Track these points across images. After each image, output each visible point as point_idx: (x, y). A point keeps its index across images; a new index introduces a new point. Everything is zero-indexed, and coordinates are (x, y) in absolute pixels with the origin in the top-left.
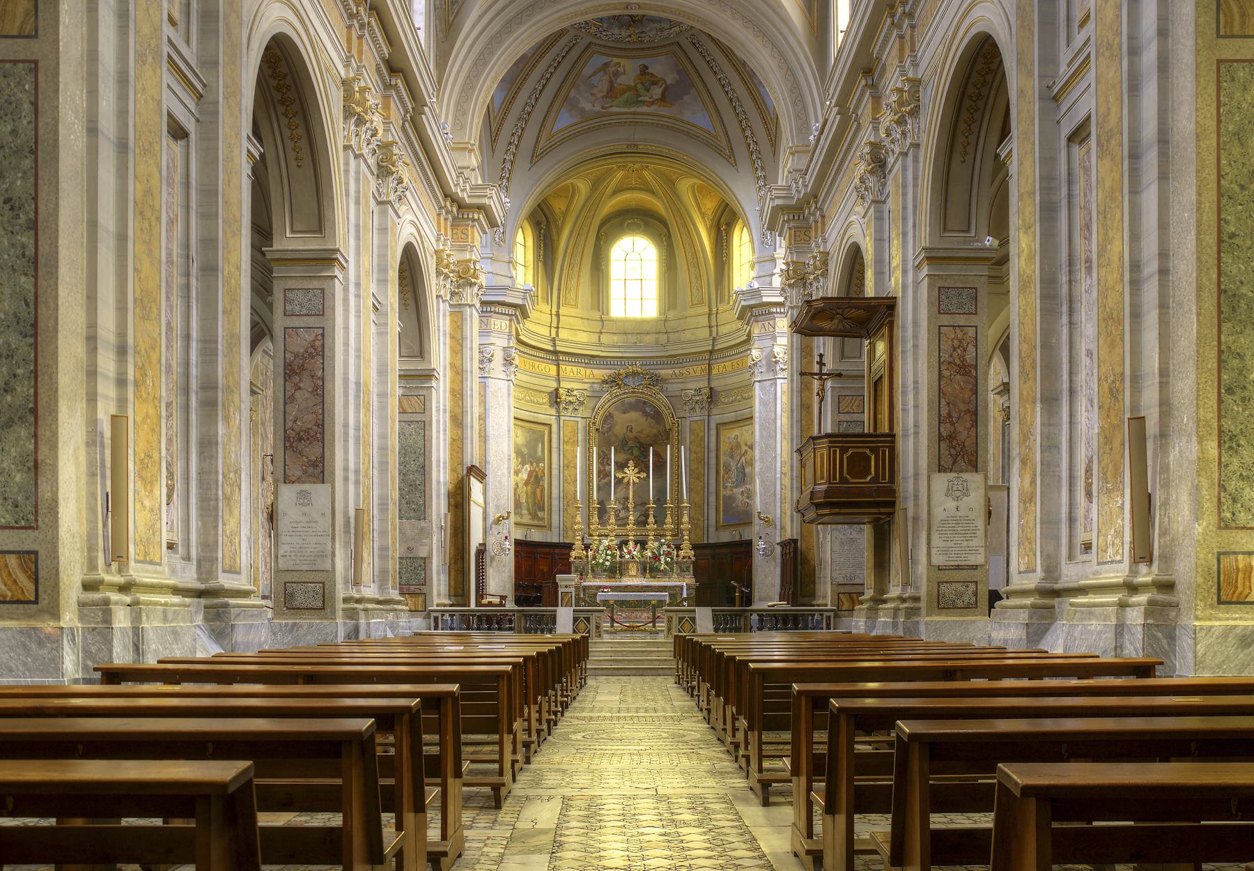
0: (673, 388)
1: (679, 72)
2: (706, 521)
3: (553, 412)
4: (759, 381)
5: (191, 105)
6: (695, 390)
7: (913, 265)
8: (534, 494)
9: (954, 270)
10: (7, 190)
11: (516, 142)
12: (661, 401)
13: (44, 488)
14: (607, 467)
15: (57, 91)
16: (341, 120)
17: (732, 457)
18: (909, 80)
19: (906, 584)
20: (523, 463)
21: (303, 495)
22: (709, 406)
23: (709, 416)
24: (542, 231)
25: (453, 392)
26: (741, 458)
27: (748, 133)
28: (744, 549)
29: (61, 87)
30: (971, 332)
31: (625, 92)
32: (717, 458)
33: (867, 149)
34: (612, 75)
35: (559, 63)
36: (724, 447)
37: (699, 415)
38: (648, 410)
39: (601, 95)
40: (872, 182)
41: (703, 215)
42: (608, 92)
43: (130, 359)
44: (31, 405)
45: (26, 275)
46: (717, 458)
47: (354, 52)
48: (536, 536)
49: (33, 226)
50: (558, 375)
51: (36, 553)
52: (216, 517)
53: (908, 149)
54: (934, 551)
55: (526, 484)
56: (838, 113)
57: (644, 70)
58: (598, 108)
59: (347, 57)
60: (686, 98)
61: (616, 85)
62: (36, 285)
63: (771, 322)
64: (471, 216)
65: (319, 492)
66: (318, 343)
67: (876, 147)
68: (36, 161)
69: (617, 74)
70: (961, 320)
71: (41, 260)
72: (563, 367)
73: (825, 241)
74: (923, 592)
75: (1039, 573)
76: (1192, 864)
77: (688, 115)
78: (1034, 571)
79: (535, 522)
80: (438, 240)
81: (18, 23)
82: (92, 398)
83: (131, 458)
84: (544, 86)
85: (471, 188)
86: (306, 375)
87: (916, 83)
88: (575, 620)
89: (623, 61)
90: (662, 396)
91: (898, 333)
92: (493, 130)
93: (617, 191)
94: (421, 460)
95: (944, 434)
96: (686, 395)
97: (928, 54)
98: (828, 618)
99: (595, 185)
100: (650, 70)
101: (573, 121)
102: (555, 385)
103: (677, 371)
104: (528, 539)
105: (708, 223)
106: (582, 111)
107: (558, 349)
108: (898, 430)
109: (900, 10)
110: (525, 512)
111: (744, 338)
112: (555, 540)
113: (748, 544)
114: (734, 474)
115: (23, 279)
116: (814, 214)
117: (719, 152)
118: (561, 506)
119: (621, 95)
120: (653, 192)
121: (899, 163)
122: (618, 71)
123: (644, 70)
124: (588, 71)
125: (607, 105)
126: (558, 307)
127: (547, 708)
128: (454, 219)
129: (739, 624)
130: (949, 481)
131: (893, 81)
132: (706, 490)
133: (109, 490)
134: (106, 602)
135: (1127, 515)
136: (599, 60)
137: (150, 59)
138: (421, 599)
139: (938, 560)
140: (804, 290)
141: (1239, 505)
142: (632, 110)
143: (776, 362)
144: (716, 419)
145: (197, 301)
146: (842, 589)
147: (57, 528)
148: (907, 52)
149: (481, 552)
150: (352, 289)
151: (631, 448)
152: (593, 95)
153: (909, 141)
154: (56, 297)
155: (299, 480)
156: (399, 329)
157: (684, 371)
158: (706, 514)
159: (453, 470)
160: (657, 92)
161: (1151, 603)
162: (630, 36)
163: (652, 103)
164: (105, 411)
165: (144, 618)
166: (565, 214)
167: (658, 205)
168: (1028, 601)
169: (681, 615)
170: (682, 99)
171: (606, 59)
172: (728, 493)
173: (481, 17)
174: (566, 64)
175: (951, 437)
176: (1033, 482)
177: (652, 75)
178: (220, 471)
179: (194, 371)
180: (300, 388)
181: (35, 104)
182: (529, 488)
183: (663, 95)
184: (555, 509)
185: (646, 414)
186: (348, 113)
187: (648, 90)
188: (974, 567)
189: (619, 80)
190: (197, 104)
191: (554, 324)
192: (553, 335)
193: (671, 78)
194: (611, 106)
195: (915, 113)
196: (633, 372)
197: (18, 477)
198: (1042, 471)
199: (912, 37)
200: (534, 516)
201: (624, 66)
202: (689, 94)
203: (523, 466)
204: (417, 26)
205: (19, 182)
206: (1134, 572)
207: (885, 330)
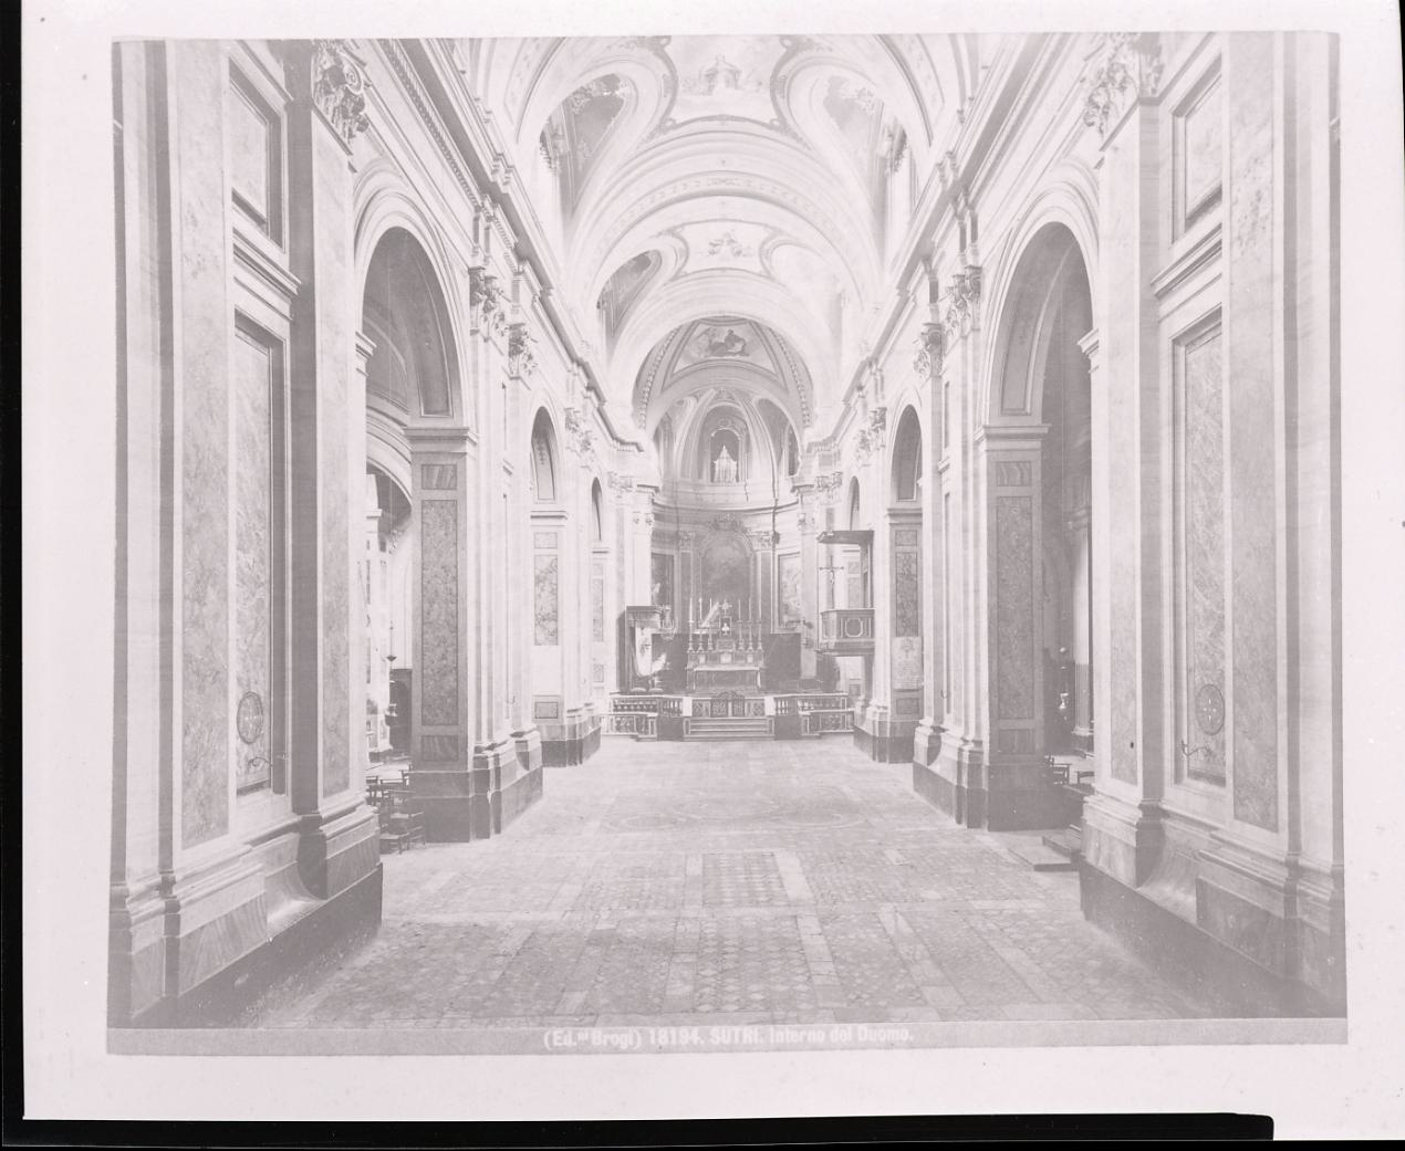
18: (971, 267)
30: (914, 556)
49: (455, 579)
72: (785, 50)
76: (1077, 874)
80: (475, 253)
86: (547, 583)
87: (977, 270)
144: (777, 553)
146: (902, 695)
171: (707, 327)
175: (903, 616)
195: (883, 428)
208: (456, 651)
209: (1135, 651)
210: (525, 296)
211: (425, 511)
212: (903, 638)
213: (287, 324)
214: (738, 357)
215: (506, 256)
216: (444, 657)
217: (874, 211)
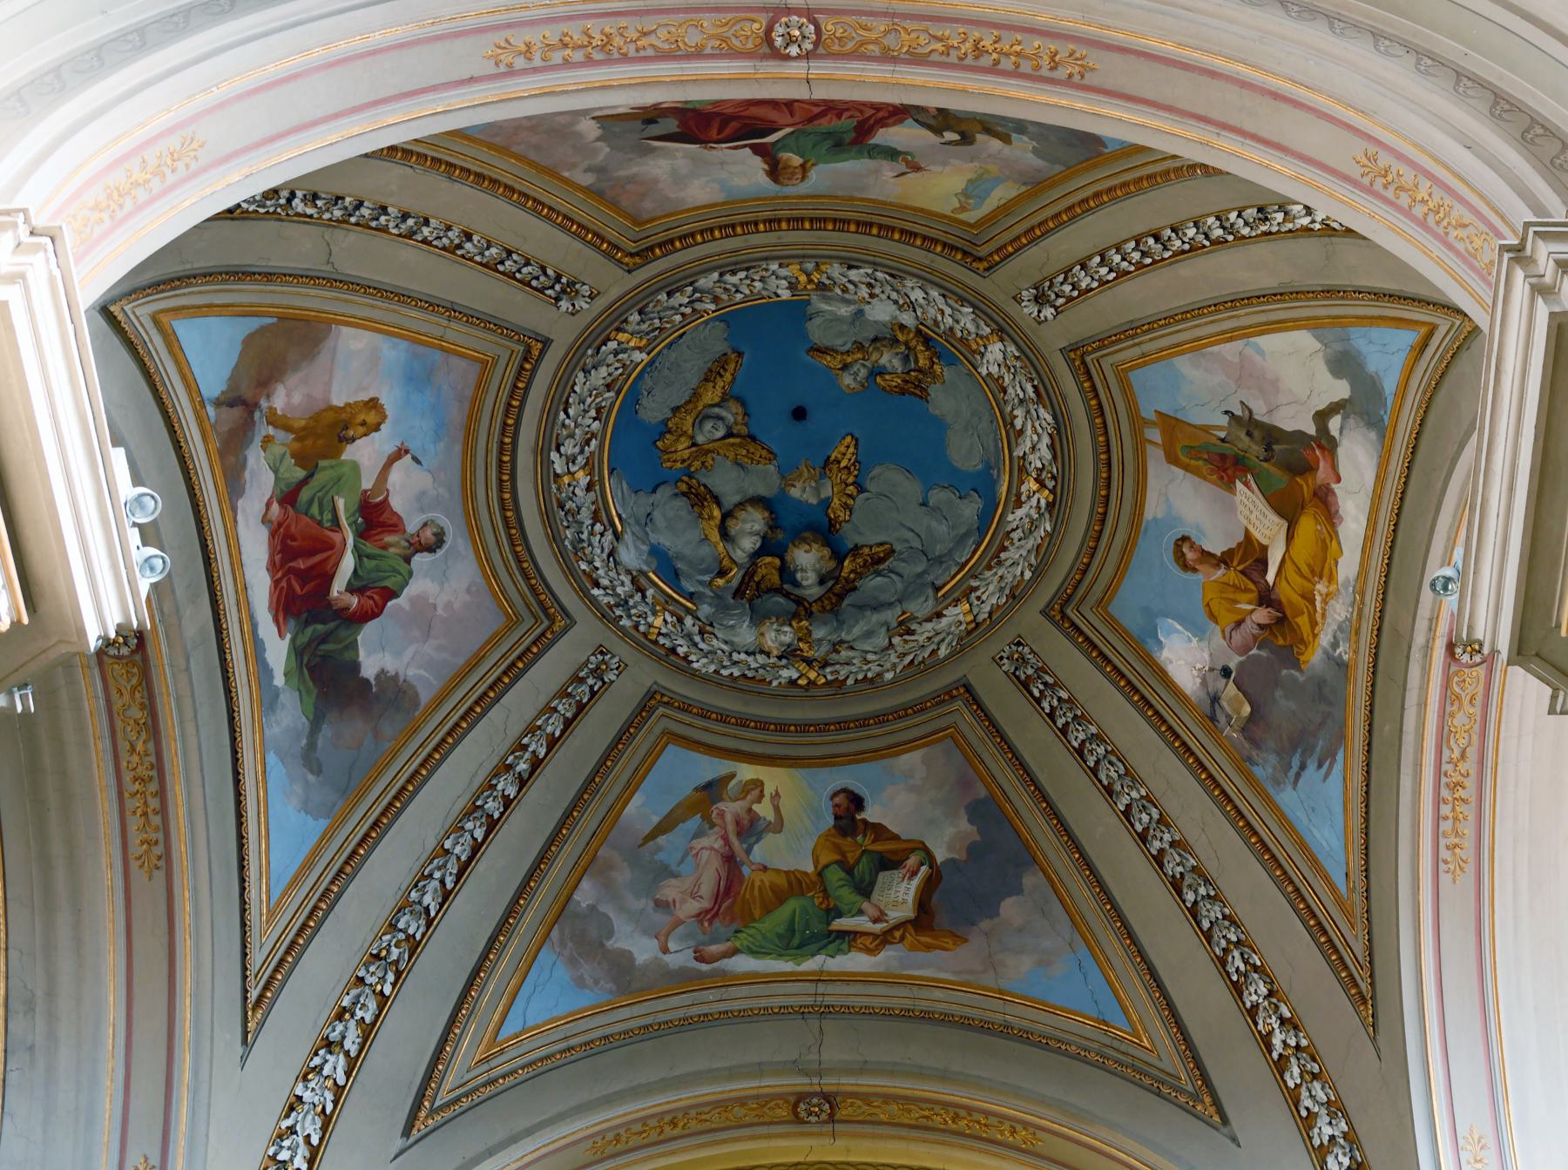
1: (977, 812)
11: (351, 1045)
31: (780, 897)
34: (731, 828)
35: (536, 764)
39: (694, 906)
42: (718, 897)
58: (680, 957)
61: (746, 870)
69: (750, 829)
77: (1019, 971)
84: (476, 848)
85: (15, 225)
89: (773, 778)
92: (257, 958)
100: (871, 814)
101: (586, 999)
106: (621, 969)
117: (1157, 1085)
119: (768, 910)
122: (754, 818)
124: (642, 810)
125: (715, 948)
127: (925, 1120)
142: (811, 964)
152: (663, 905)
170: (994, 913)
177: (879, 831)
183: (923, 904)
187: (865, 890)
189: (759, 853)
194: (735, 952)
201: (776, 796)
202: (1018, 890)
214: (887, 959)
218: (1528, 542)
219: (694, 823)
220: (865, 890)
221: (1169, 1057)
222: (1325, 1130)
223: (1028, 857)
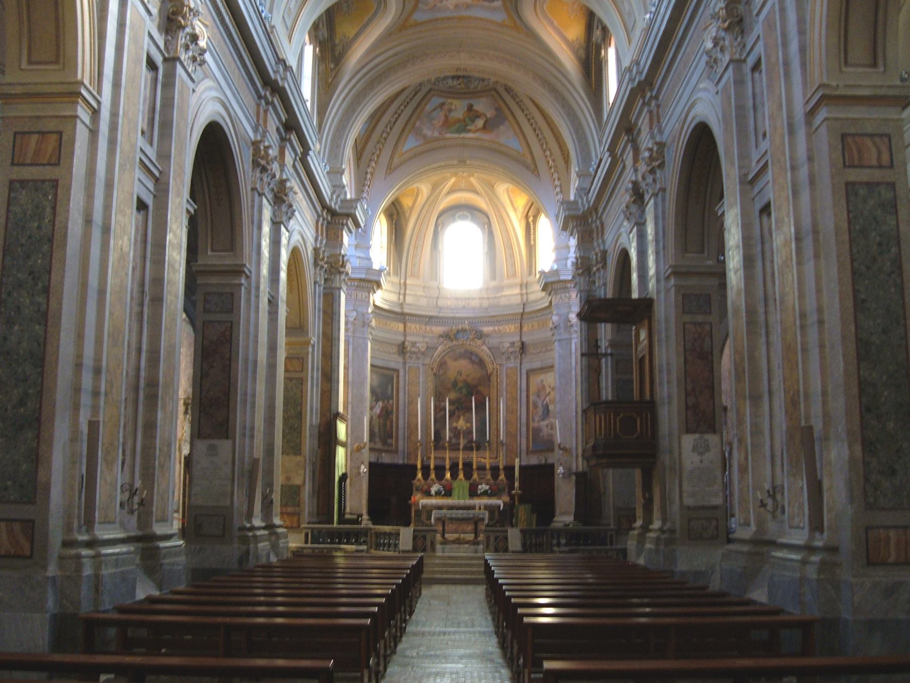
0: (493, 341)
2: (519, 447)
3: (401, 360)
4: (559, 340)
5: (151, 186)
6: (510, 343)
7: (664, 276)
8: (385, 425)
9: (692, 282)
10: (31, 266)
12: (484, 351)
13: (41, 473)
14: (442, 404)
15: (69, 200)
16: (251, 170)
17: (539, 396)
18: (657, 143)
19: (664, 520)
20: (377, 401)
21: (213, 450)
22: (521, 356)
23: (521, 364)
24: (394, 221)
25: (324, 355)
26: (546, 397)
27: (548, 153)
28: (548, 470)
29: (72, 197)
30: (707, 327)
32: (528, 397)
33: (630, 186)
35: (408, 103)
36: (533, 389)
37: (513, 363)
38: (473, 358)
40: (634, 209)
41: (515, 210)
43: (103, 377)
44: (36, 415)
45: (40, 324)
46: (528, 397)
47: (261, 122)
48: (386, 459)
49: (46, 290)
50: (405, 330)
51: (33, 521)
52: (153, 481)
53: (658, 192)
54: (685, 495)
55: (379, 416)
56: (609, 156)
57: (470, 108)
58: (436, 134)
59: (256, 125)
60: (502, 128)
62: (46, 332)
63: (567, 295)
64: (341, 221)
65: (224, 446)
66: (227, 333)
67: (635, 184)
68: (52, 247)
69: (450, 111)
70: (700, 318)
71: (50, 314)
72: (409, 325)
73: (604, 242)
74: (678, 525)
75: (753, 528)
78: (749, 525)
79: (386, 448)
81: (48, 156)
82: (76, 408)
83: (100, 449)
88: (415, 538)
89: (455, 102)
90: (484, 348)
91: (655, 325)
92: (358, 150)
93: (449, 192)
94: (299, 408)
95: (690, 404)
96: (503, 347)
97: (670, 126)
98: (611, 536)
99: (434, 187)
102: (402, 339)
103: (496, 328)
104: (380, 461)
105: (520, 216)
106: (425, 137)
107: (406, 311)
108: (658, 397)
109: (648, 95)
110: (377, 440)
111: (547, 304)
112: (401, 462)
113: (551, 468)
114: (540, 410)
115: (37, 327)
116: (595, 221)
117: (527, 167)
118: (406, 434)
120: (476, 192)
121: (652, 201)
123: (470, 108)
124: (429, 108)
126: (406, 279)
128: (328, 223)
129: (543, 539)
130: (695, 440)
131: (646, 141)
132: (519, 422)
133: (84, 472)
134: (79, 557)
135: (806, 494)
136: (437, 101)
137: (128, 166)
138: (296, 518)
139: (688, 501)
140: (589, 278)
141: (879, 492)
143: (571, 326)
144: (526, 366)
145: (148, 323)
147: (48, 504)
148: (655, 123)
149: (344, 477)
150: (253, 291)
151: (461, 388)
153: (658, 186)
154: (59, 340)
155: (209, 437)
156: (286, 314)
157: (501, 328)
158: (519, 441)
159: (322, 415)
160: (480, 123)
161: (823, 563)
162: (460, 84)
163: (477, 131)
164: (84, 418)
165: (103, 567)
166: (412, 208)
167: (481, 203)
168: (745, 548)
169: (498, 534)
171: (441, 100)
172: (536, 425)
173: (350, 80)
174: (414, 103)
176: (746, 458)
177: (476, 111)
178: (158, 446)
179: (143, 374)
180: (213, 367)
181: (54, 208)
182: (381, 420)
184: (401, 436)
185: (473, 362)
186: (256, 164)
188: (715, 508)
189: (452, 114)
190: (155, 185)
191: (402, 292)
192: (401, 300)
193: (490, 113)
195: (661, 166)
196: (462, 329)
197: (24, 467)
198: (752, 450)
199: (658, 112)
200: (384, 442)
203: (377, 403)
204: (305, 98)
205: (39, 261)
206: (811, 537)
207: (646, 322)
208: (40, 393)
209: (123, 358)
210: (289, 158)
211: (12, 195)
212: (697, 436)
213: (152, 197)
214: (477, 135)
215: (278, 130)
216: (22, 403)
217: (583, 75)
218: (601, 77)
219: (439, 109)
220: (473, 121)
221: (529, 161)
222: (557, 182)
223: (506, 118)
